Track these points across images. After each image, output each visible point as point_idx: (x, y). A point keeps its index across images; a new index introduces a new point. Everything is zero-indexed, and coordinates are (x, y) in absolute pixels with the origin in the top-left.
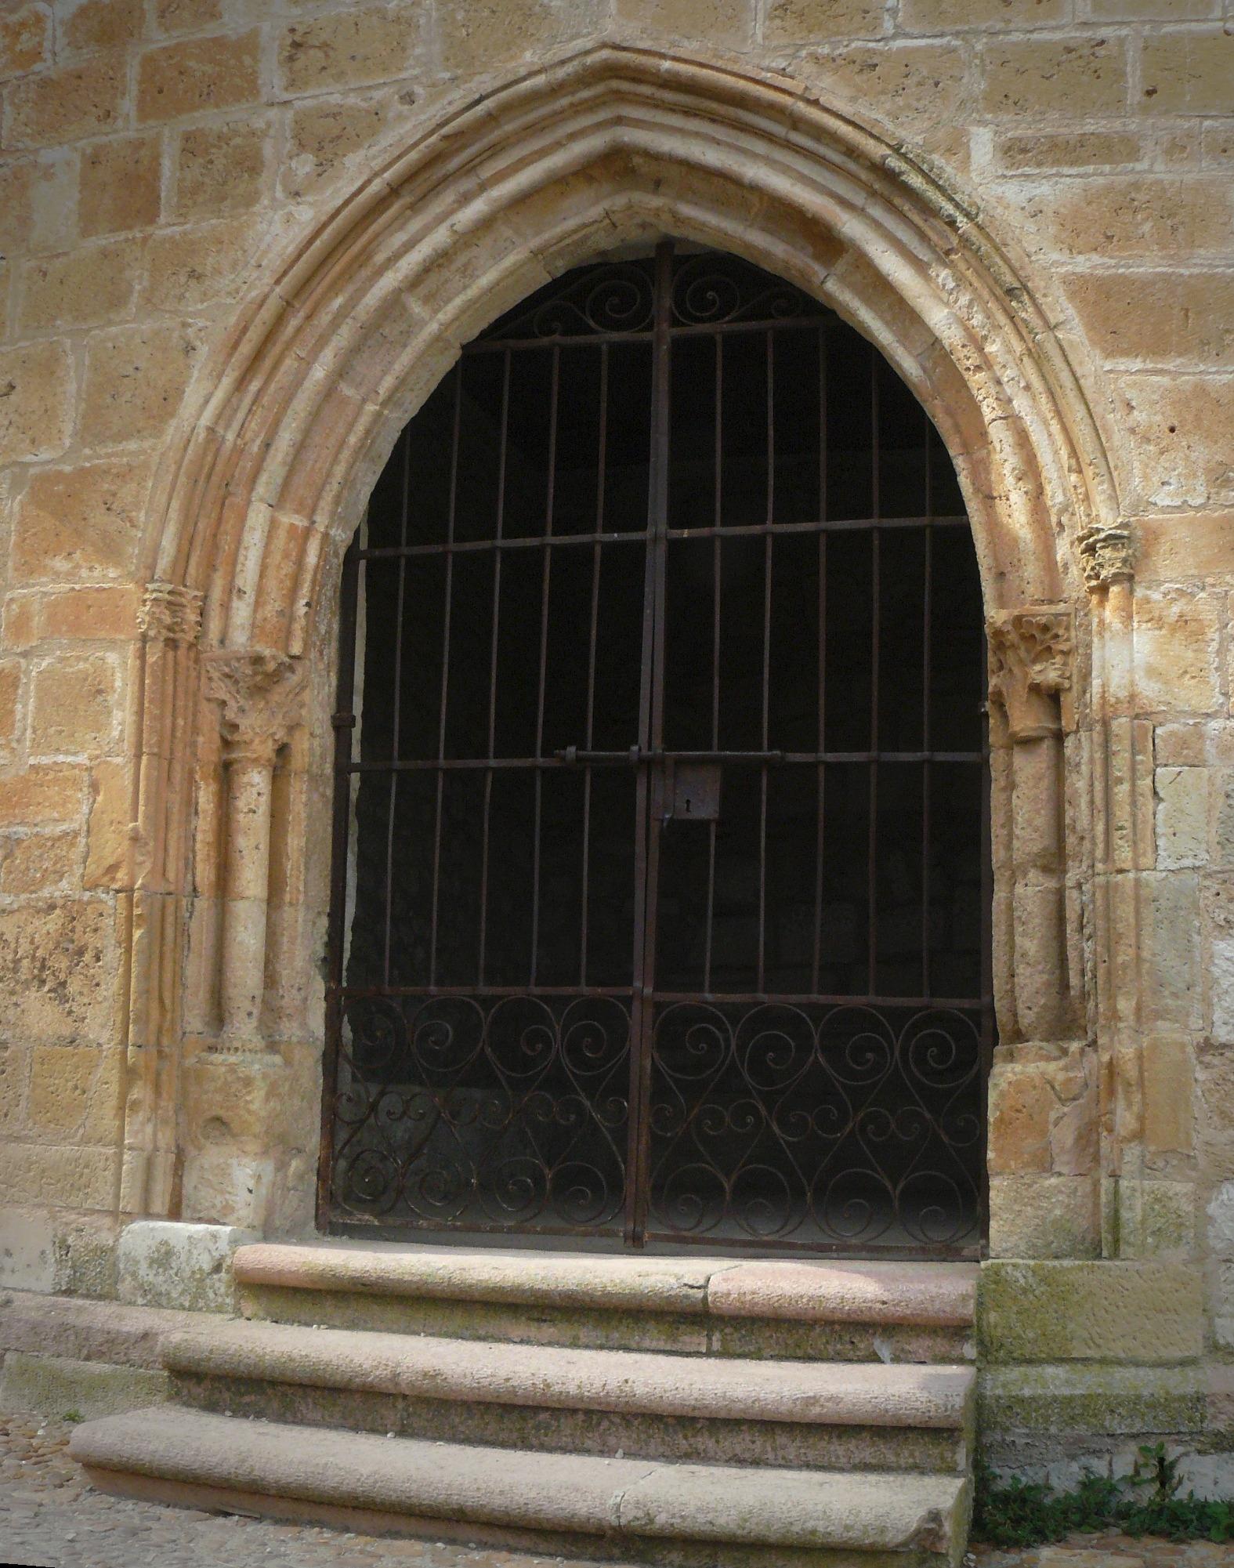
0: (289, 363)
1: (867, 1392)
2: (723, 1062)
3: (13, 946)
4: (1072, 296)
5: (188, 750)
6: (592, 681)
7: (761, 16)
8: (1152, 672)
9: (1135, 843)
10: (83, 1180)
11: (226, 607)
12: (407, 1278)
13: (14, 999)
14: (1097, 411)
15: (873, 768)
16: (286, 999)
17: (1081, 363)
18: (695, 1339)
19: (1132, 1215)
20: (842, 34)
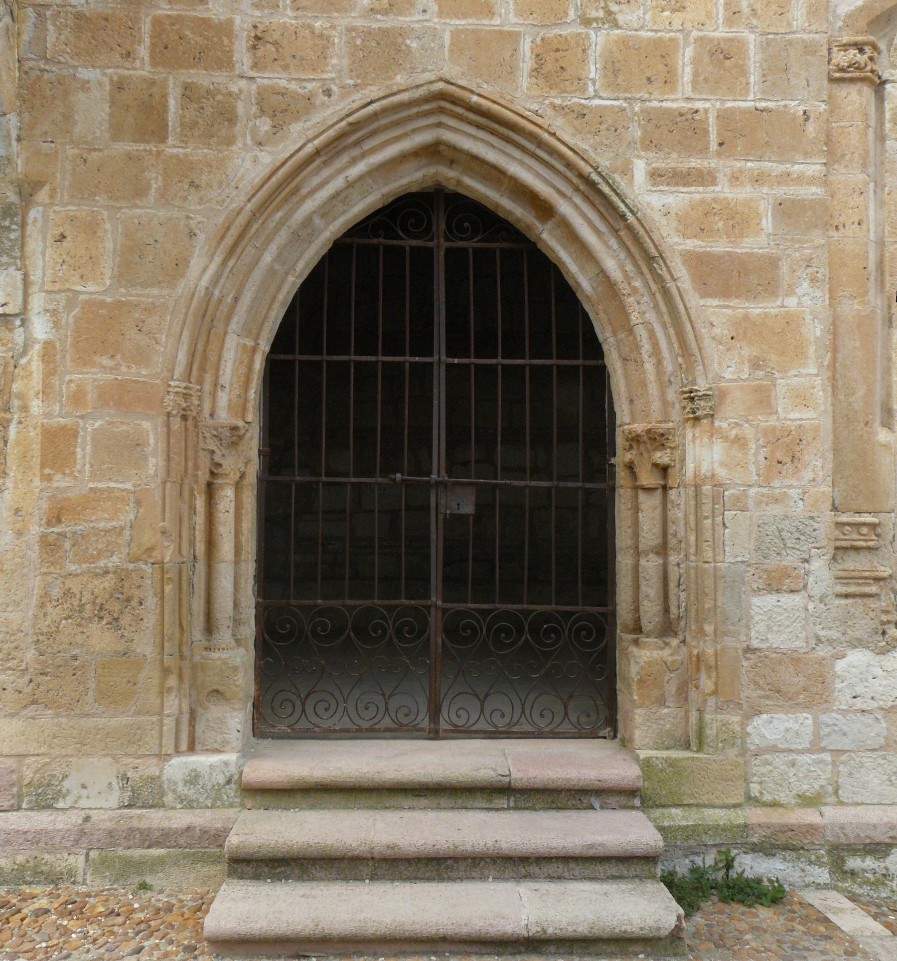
7: (525, 75)
8: (723, 464)
9: (714, 548)
10: (137, 737)
11: (214, 395)
12: (348, 780)
14: (697, 326)
18: (502, 801)
20: (567, 92)
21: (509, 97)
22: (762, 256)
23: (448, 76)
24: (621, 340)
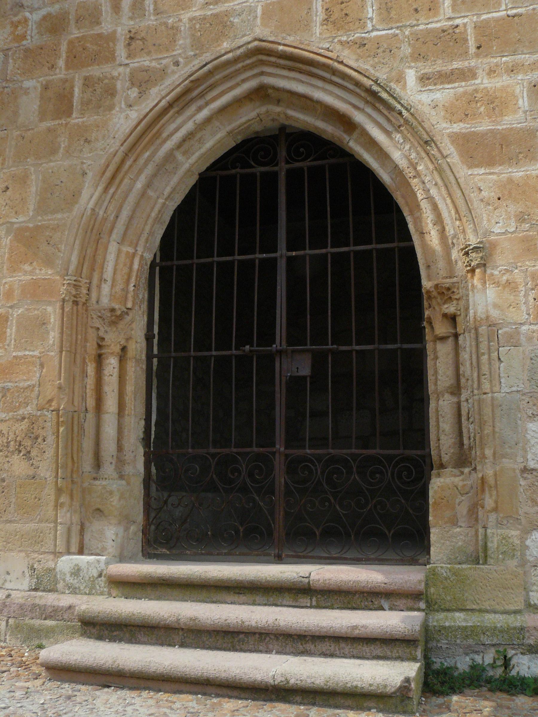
0: (126, 181)
1: (378, 624)
3: (6, 436)
4: (453, 142)
5: (83, 349)
6: (255, 318)
7: (318, 24)
9: (491, 381)
10: (40, 539)
11: (99, 287)
12: (182, 576)
13: (7, 459)
14: (466, 192)
15: (376, 351)
17: (458, 172)
18: (305, 601)
19: (493, 545)
20: (351, 31)
22: (521, 129)
23: (261, 37)
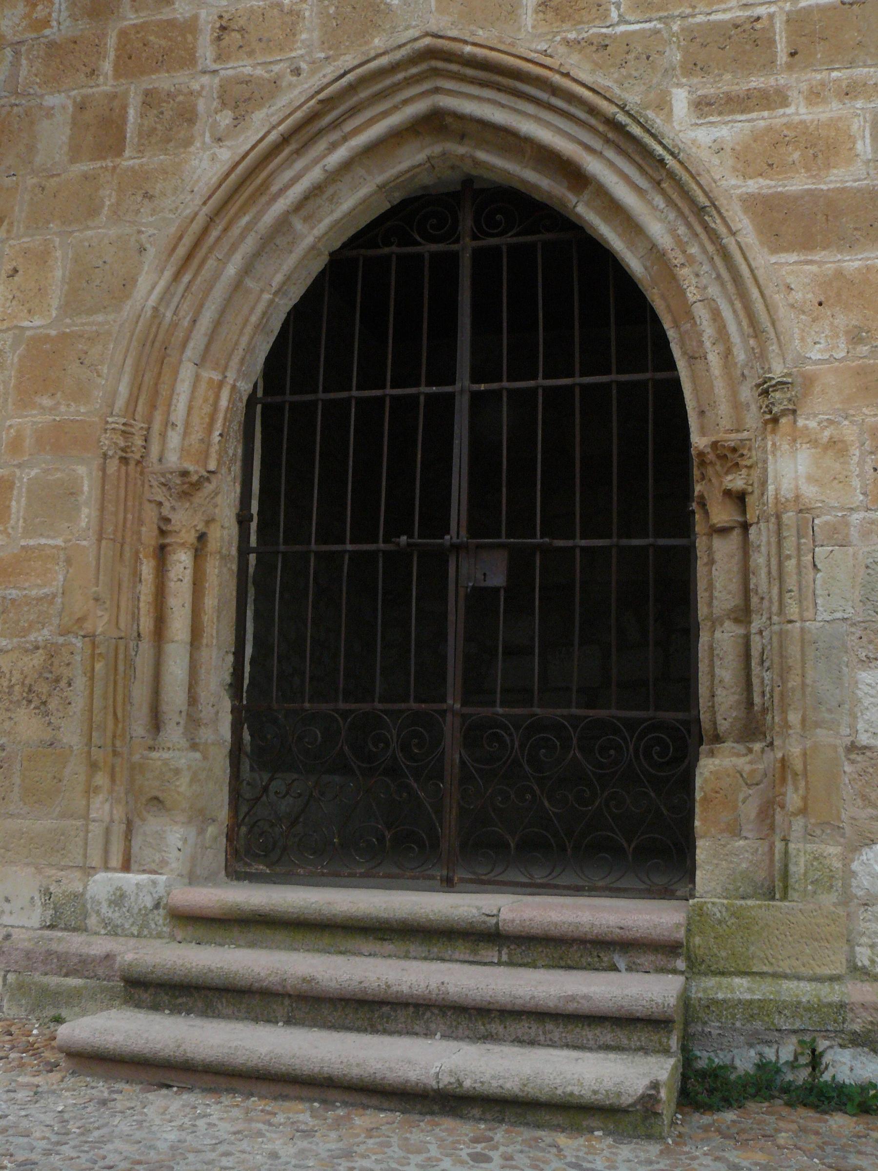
0: (211, 263)
2: (508, 758)
4: (746, 210)
7: (530, 12)
8: (810, 479)
9: (800, 601)
11: (163, 435)
12: (290, 910)
14: (767, 292)
15: (614, 551)
16: (204, 713)
18: (490, 953)
19: (798, 869)
20: (583, 23)
21: (509, 40)
22: (859, 190)
23: (434, 29)
24: (686, 332)
